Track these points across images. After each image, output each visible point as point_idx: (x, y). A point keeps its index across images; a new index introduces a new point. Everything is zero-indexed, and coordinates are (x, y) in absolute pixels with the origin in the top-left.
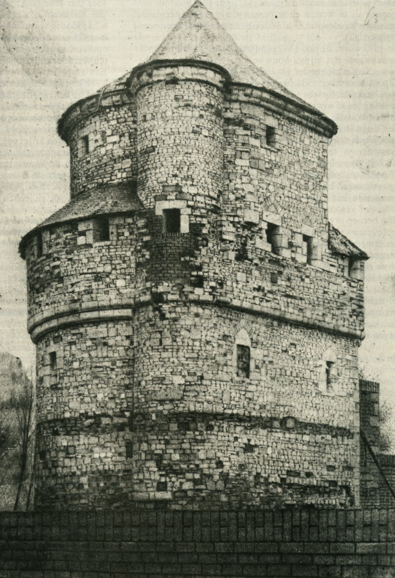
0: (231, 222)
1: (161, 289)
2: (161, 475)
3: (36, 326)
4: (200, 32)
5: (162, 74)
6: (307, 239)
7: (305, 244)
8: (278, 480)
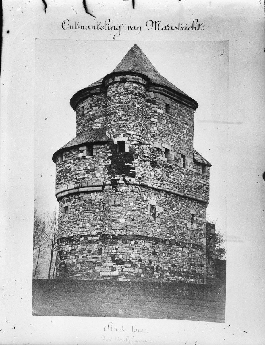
0: (148, 148)
1: (116, 178)
2: (114, 265)
3: (58, 193)
4: (52, 213)
5: (117, 79)
6: (183, 156)
7: (182, 159)
8: (167, 269)
